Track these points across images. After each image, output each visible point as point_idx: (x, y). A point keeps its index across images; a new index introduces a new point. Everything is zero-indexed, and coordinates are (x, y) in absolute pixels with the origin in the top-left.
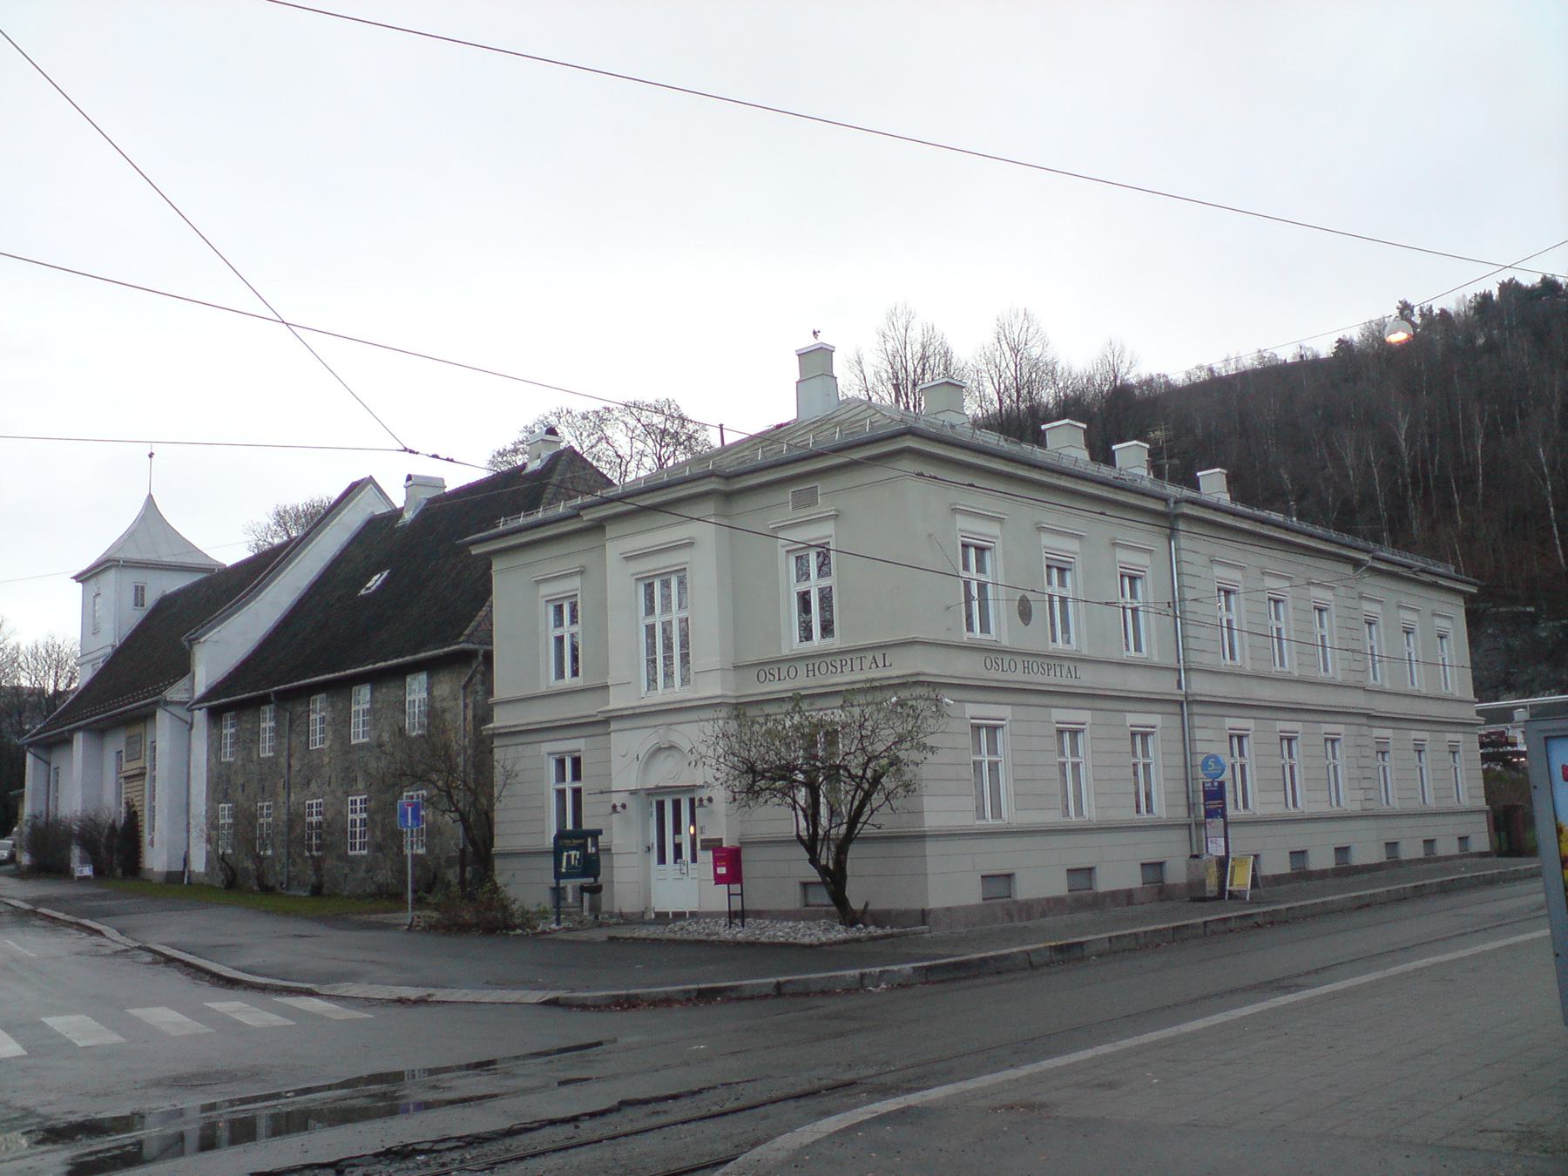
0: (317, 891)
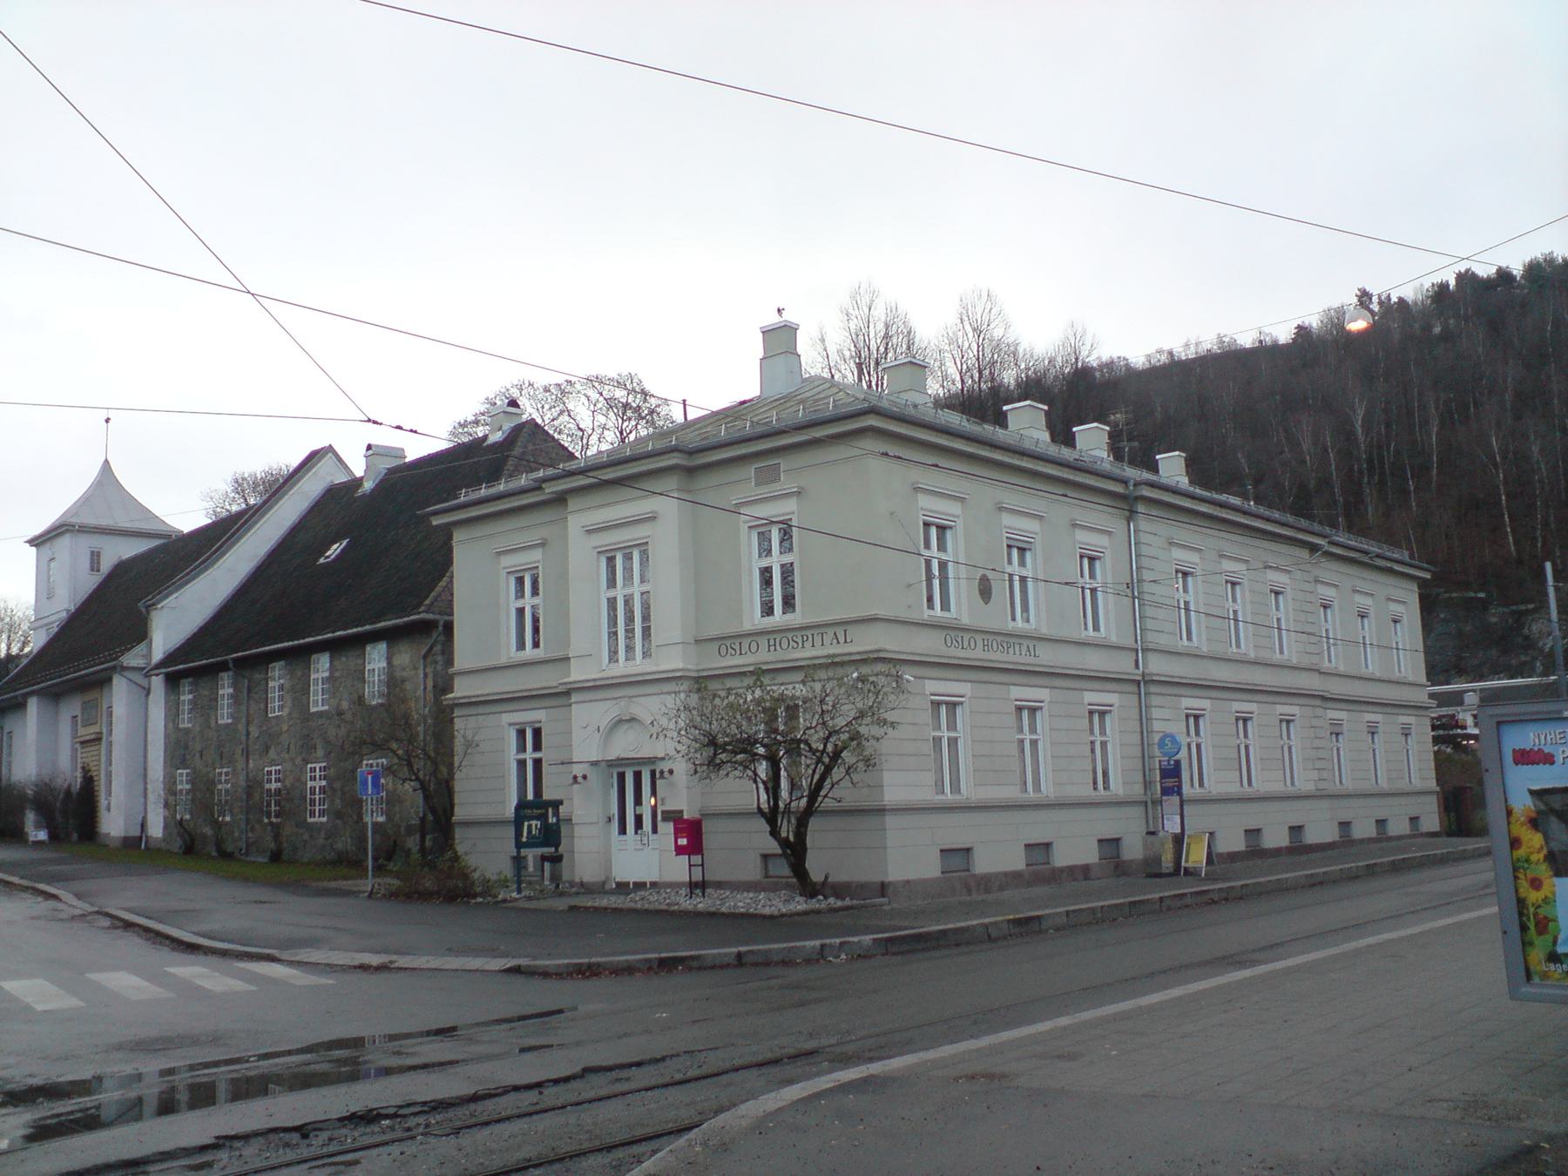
0: (276, 857)
